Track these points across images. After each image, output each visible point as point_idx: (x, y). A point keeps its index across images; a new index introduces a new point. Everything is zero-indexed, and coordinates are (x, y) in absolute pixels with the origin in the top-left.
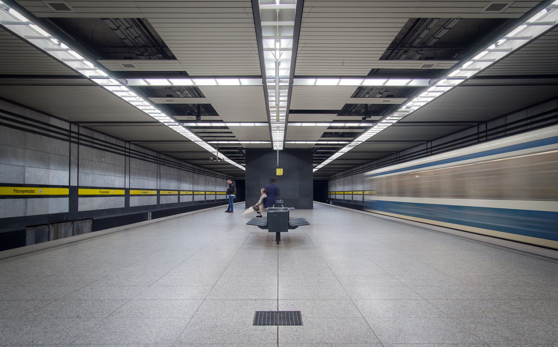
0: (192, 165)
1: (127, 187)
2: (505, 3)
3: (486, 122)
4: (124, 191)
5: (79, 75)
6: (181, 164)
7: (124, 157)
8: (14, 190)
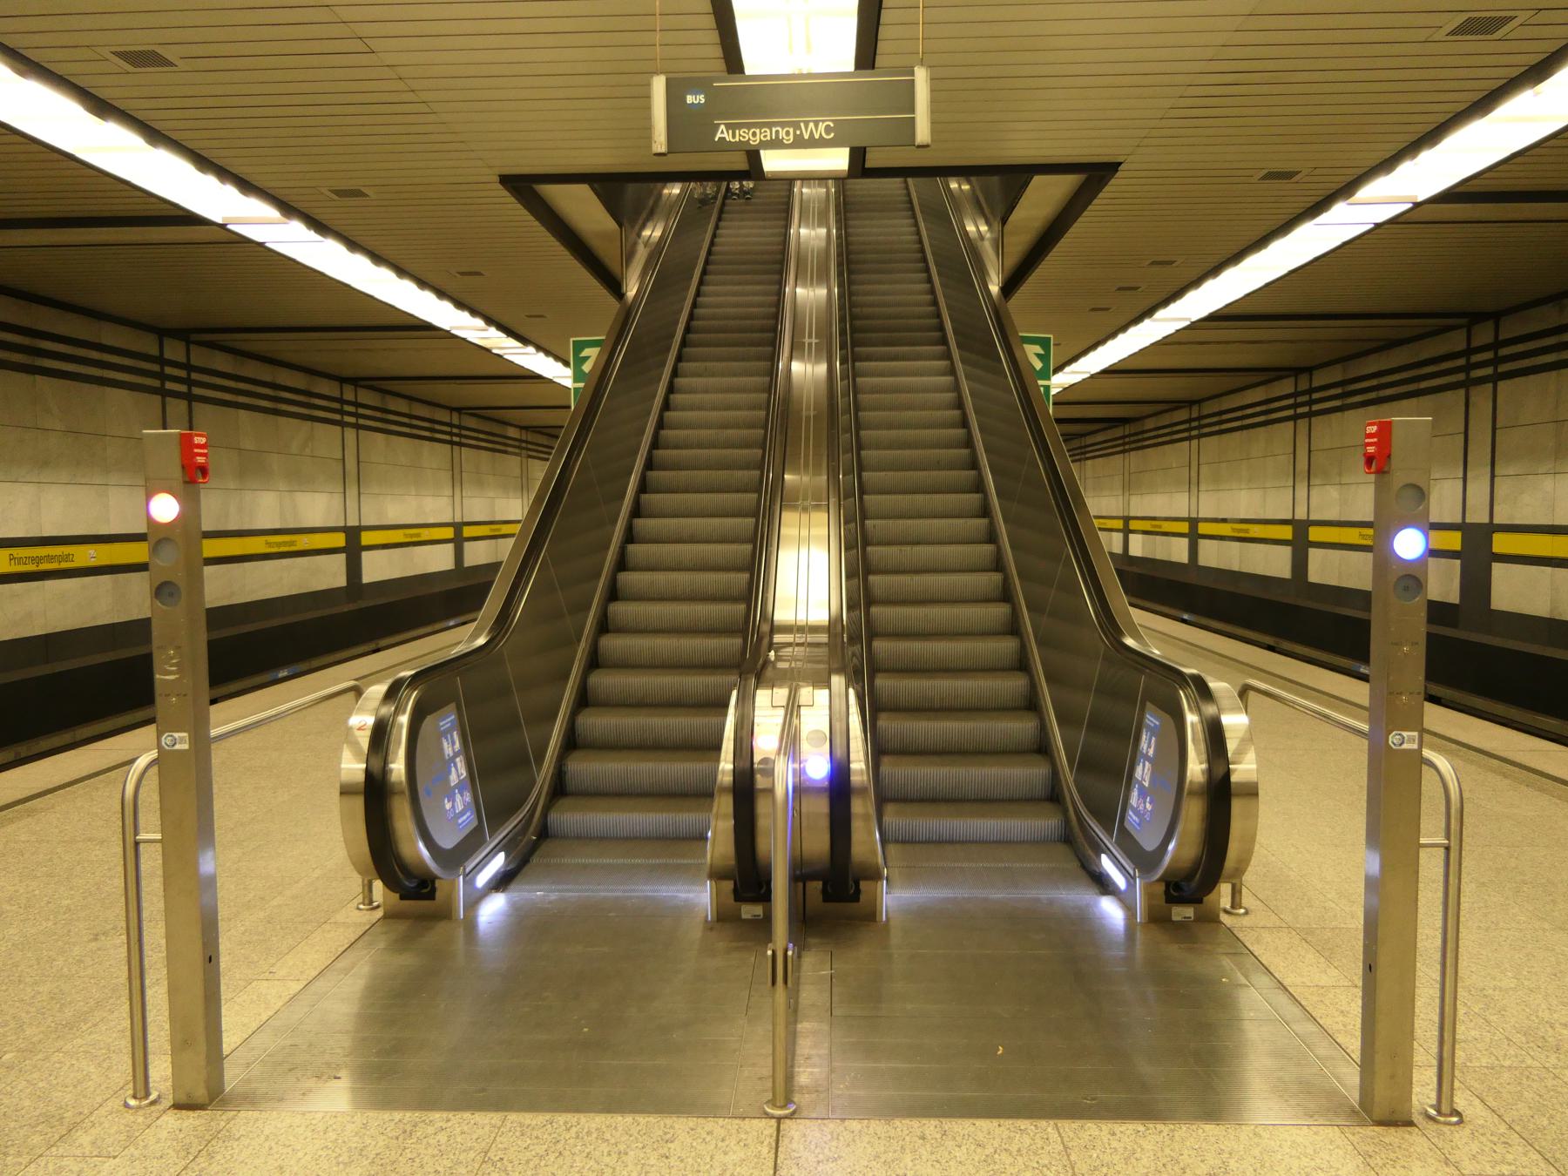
0: (518, 430)
1: (458, 519)
2: (1508, 15)
3: (1496, 316)
4: (1311, 539)
5: (184, 214)
6: (194, 362)
7: (449, 446)
8: (12, 558)
